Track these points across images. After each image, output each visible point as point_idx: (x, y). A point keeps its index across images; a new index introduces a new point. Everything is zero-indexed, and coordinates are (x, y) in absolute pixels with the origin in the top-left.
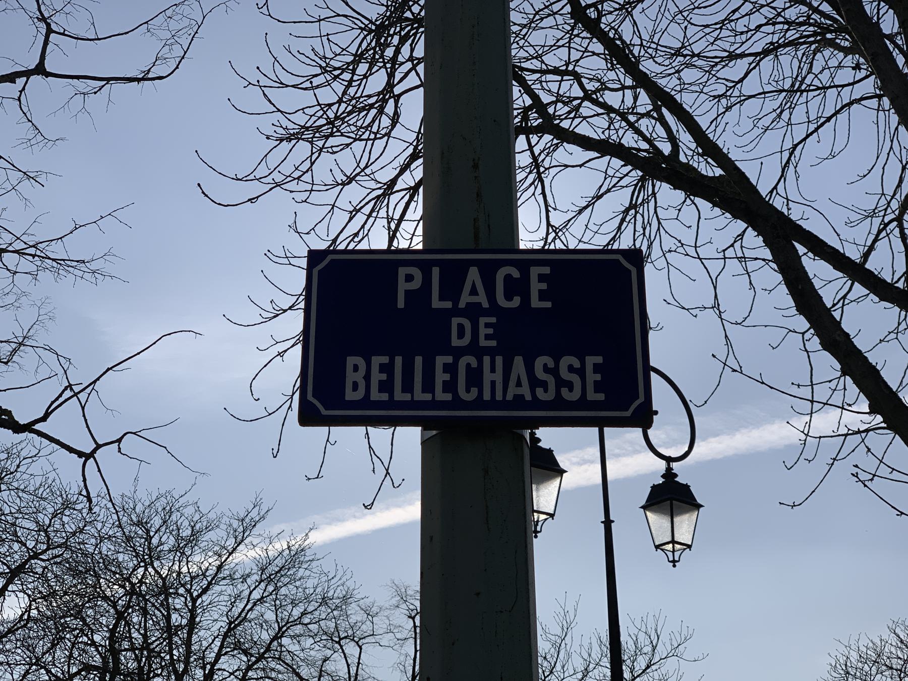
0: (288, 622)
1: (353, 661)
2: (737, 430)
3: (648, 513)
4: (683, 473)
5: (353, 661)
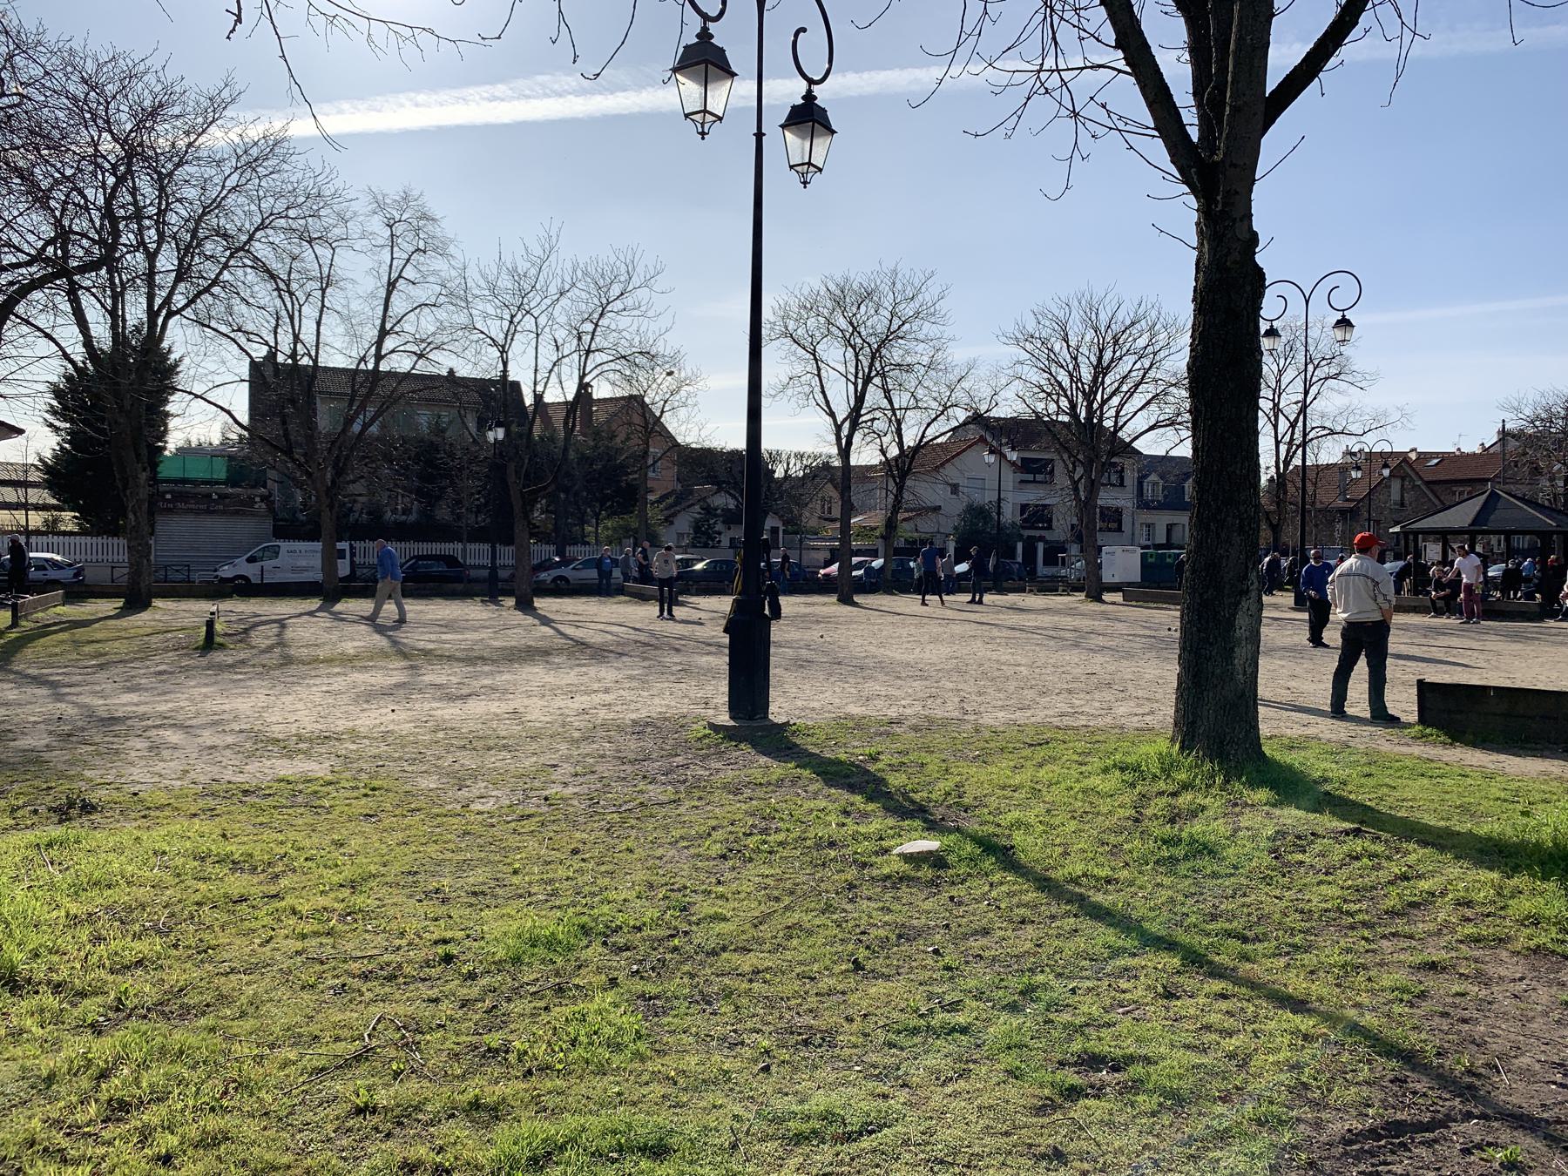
0: (271, 214)
1: (326, 262)
2: (644, 88)
3: (787, 133)
4: (821, 93)
5: (326, 262)
